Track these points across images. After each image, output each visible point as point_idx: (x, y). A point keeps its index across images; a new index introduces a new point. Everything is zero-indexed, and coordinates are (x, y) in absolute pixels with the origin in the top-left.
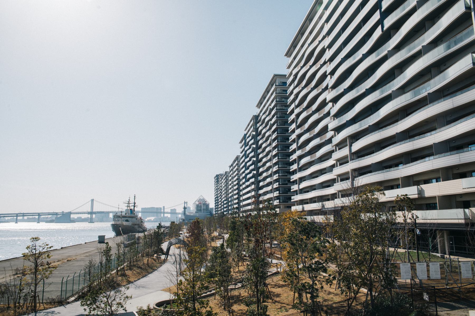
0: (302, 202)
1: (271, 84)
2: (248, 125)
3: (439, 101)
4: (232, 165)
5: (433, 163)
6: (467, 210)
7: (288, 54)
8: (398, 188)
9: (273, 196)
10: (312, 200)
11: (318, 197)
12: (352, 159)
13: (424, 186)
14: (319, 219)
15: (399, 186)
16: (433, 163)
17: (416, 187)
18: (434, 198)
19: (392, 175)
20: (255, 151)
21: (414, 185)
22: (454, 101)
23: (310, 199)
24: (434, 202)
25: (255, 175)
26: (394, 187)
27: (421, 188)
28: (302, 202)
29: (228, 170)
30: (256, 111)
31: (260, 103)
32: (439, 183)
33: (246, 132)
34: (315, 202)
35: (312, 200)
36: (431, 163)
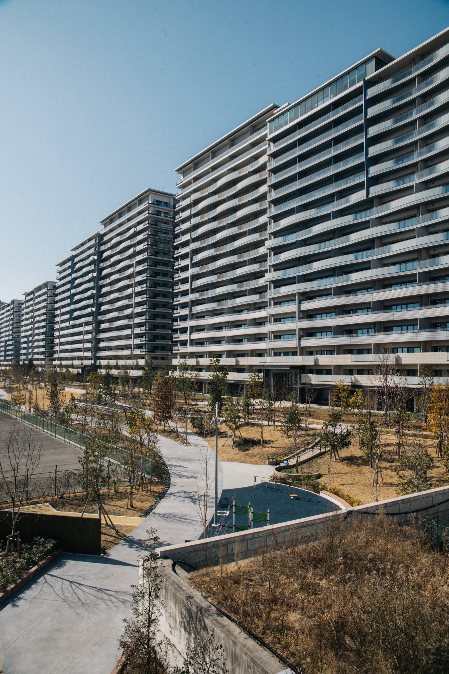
0: (61, 359)
1: (140, 200)
2: (82, 245)
3: (425, 283)
4: (32, 293)
5: (418, 335)
6: (352, 376)
7: (183, 171)
8: (368, 353)
9: (132, 343)
10: (67, 359)
11: (113, 356)
12: (300, 318)
13: (240, 359)
14: (114, 372)
15: (370, 351)
16: (418, 335)
17: (196, 359)
18: (204, 366)
19: (432, 335)
20: (96, 281)
21: (233, 357)
22: (446, 285)
23: (209, 352)
24: (330, 368)
25: (93, 313)
26: (354, 352)
27: (316, 357)
28: (61, 359)
29: (22, 298)
30: (102, 229)
31: (111, 219)
32: (333, 355)
33: (75, 253)
34: (68, 360)
35: (67, 359)
36: (445, 334)
